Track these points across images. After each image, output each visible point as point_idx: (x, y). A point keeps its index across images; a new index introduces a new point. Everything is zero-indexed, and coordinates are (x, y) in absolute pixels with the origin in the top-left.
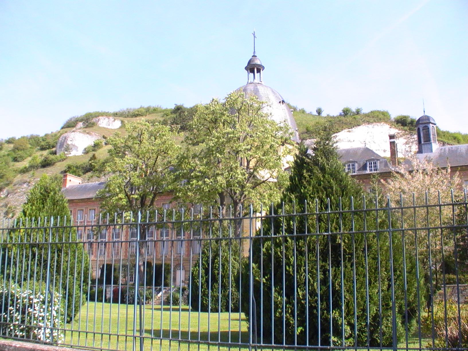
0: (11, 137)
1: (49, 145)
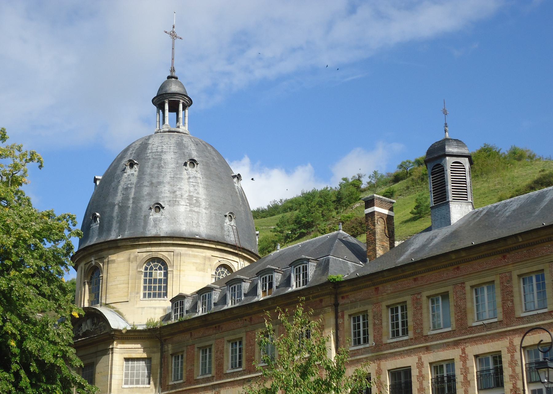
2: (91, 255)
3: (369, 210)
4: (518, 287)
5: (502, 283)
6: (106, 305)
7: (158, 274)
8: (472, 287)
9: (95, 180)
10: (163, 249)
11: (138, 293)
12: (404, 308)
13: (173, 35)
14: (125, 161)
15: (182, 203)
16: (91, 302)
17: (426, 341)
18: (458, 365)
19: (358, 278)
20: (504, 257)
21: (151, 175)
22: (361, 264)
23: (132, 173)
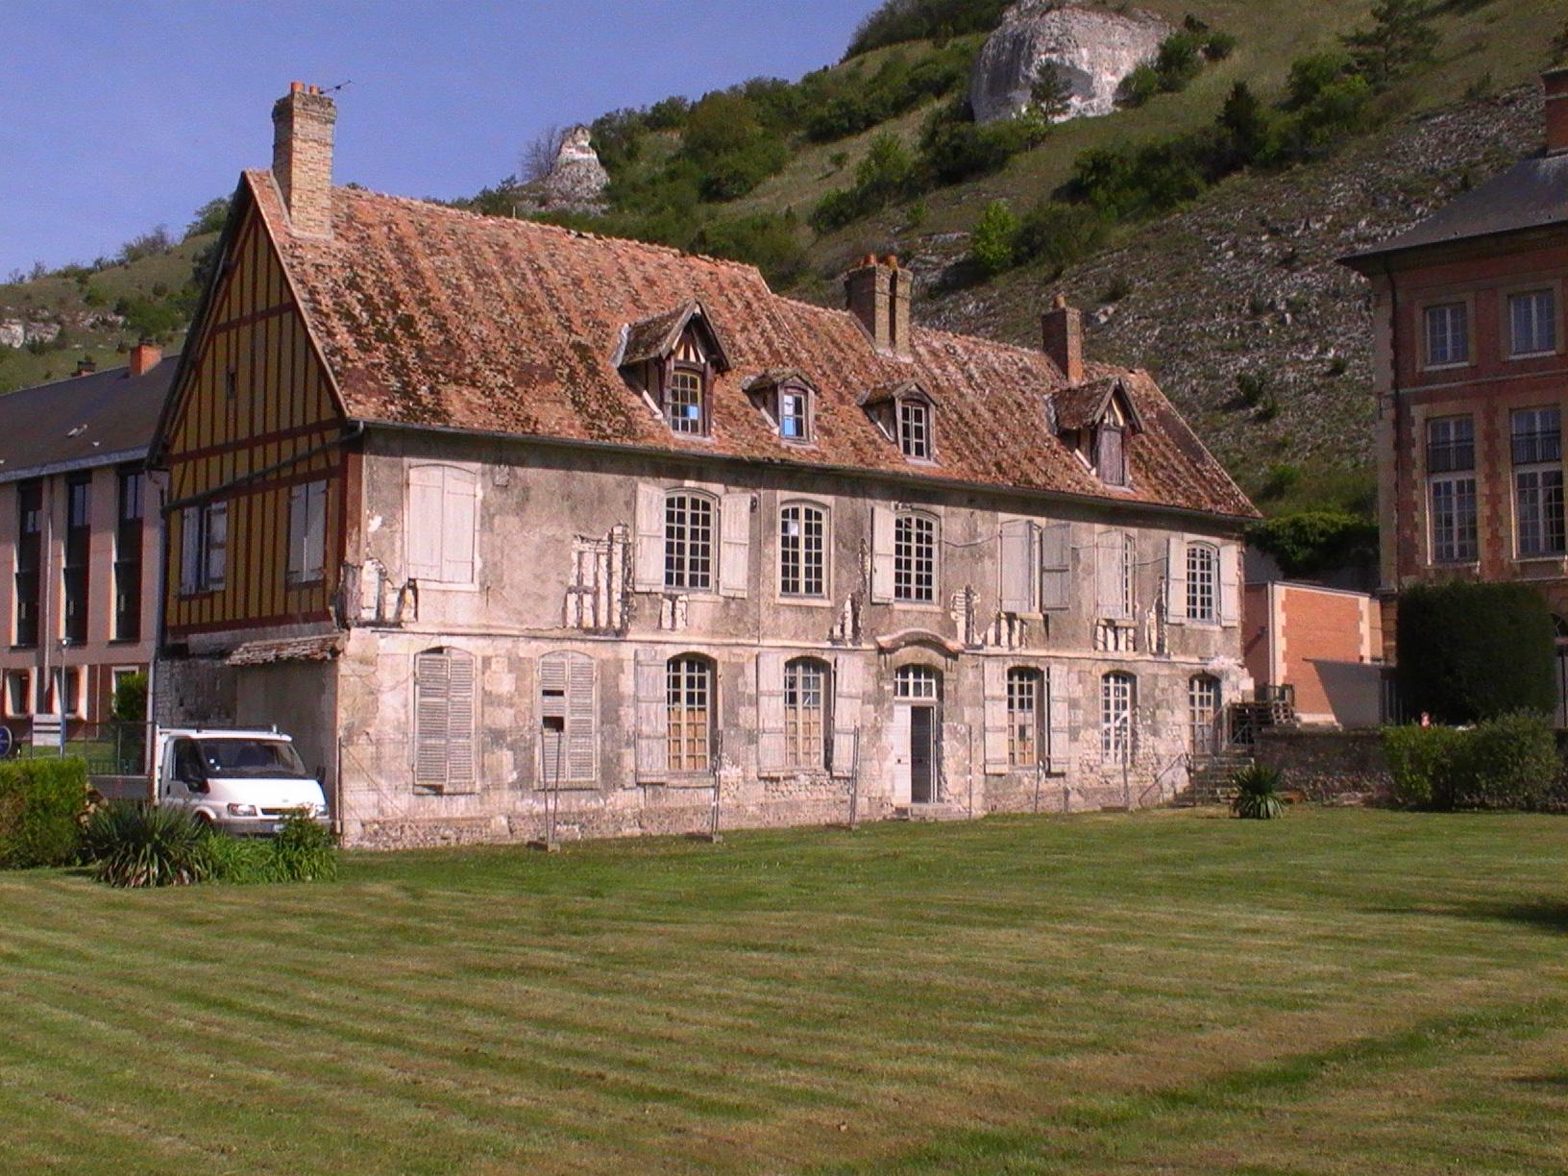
0: (663, 100)
1: (850, 115)
18: (1480, 427)
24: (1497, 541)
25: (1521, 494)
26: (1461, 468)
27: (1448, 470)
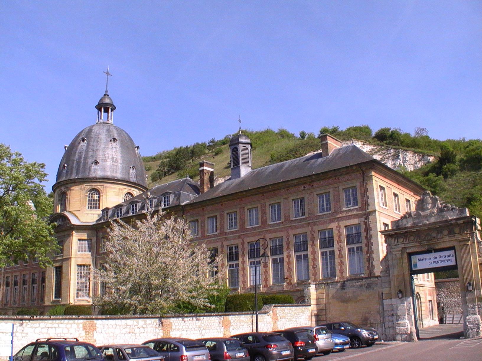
2: (62, 185)
3: (201, 168)
4: (269, 210)
5: (262, 208)
6: (69, 212)
7: (96, 197)
8: (248, 209)
9: (65, 147)
10: (99, 184)
11: (85, 206)
12: (279, 207)
13: (108, 74)
14: (80, 138)
15: (108, 160)
16: (62, 210)
17: (226, 235)
18: (240, 247)
19: (194, 203)
20: (263, 195)
21: (93, 146)
22: (197, 195)
23: (84, 144)
24: (342, 271)
25: (323, 258)
26: (357, 242)
27: (353, 243)
